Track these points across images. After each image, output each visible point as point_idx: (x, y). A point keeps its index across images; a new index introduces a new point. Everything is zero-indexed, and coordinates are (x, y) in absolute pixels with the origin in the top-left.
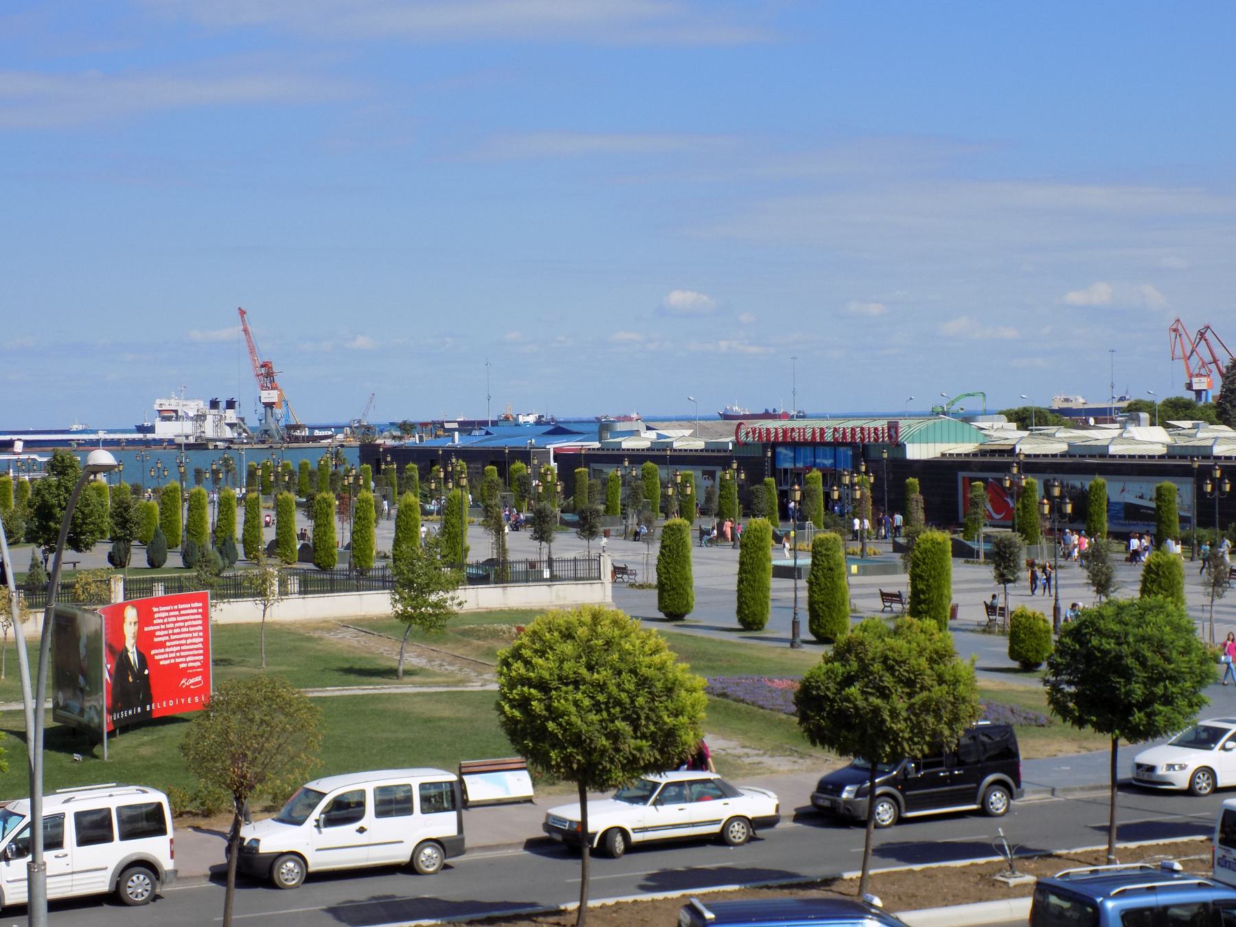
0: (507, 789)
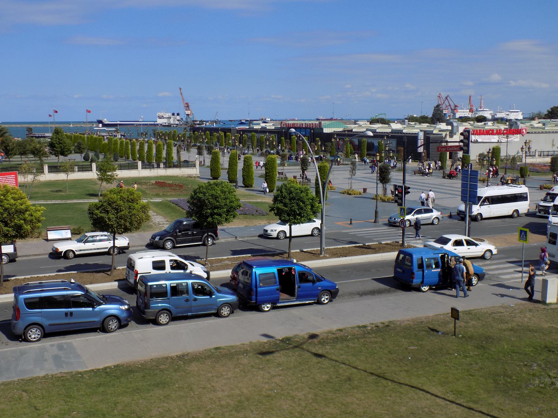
0: (62, 236)
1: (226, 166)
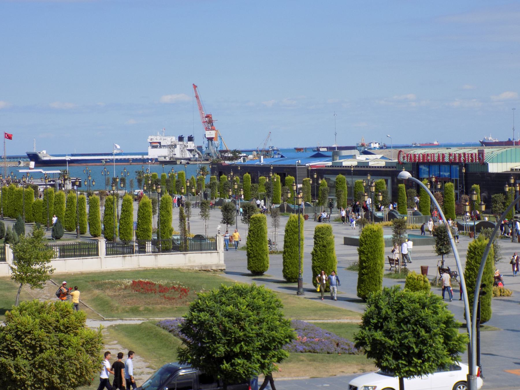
1: (280, 246)
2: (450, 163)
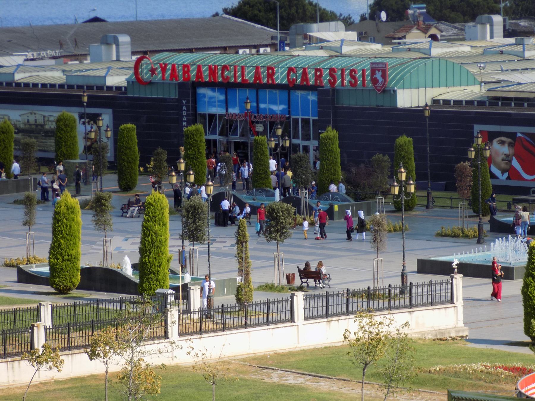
2: (291, 86)
